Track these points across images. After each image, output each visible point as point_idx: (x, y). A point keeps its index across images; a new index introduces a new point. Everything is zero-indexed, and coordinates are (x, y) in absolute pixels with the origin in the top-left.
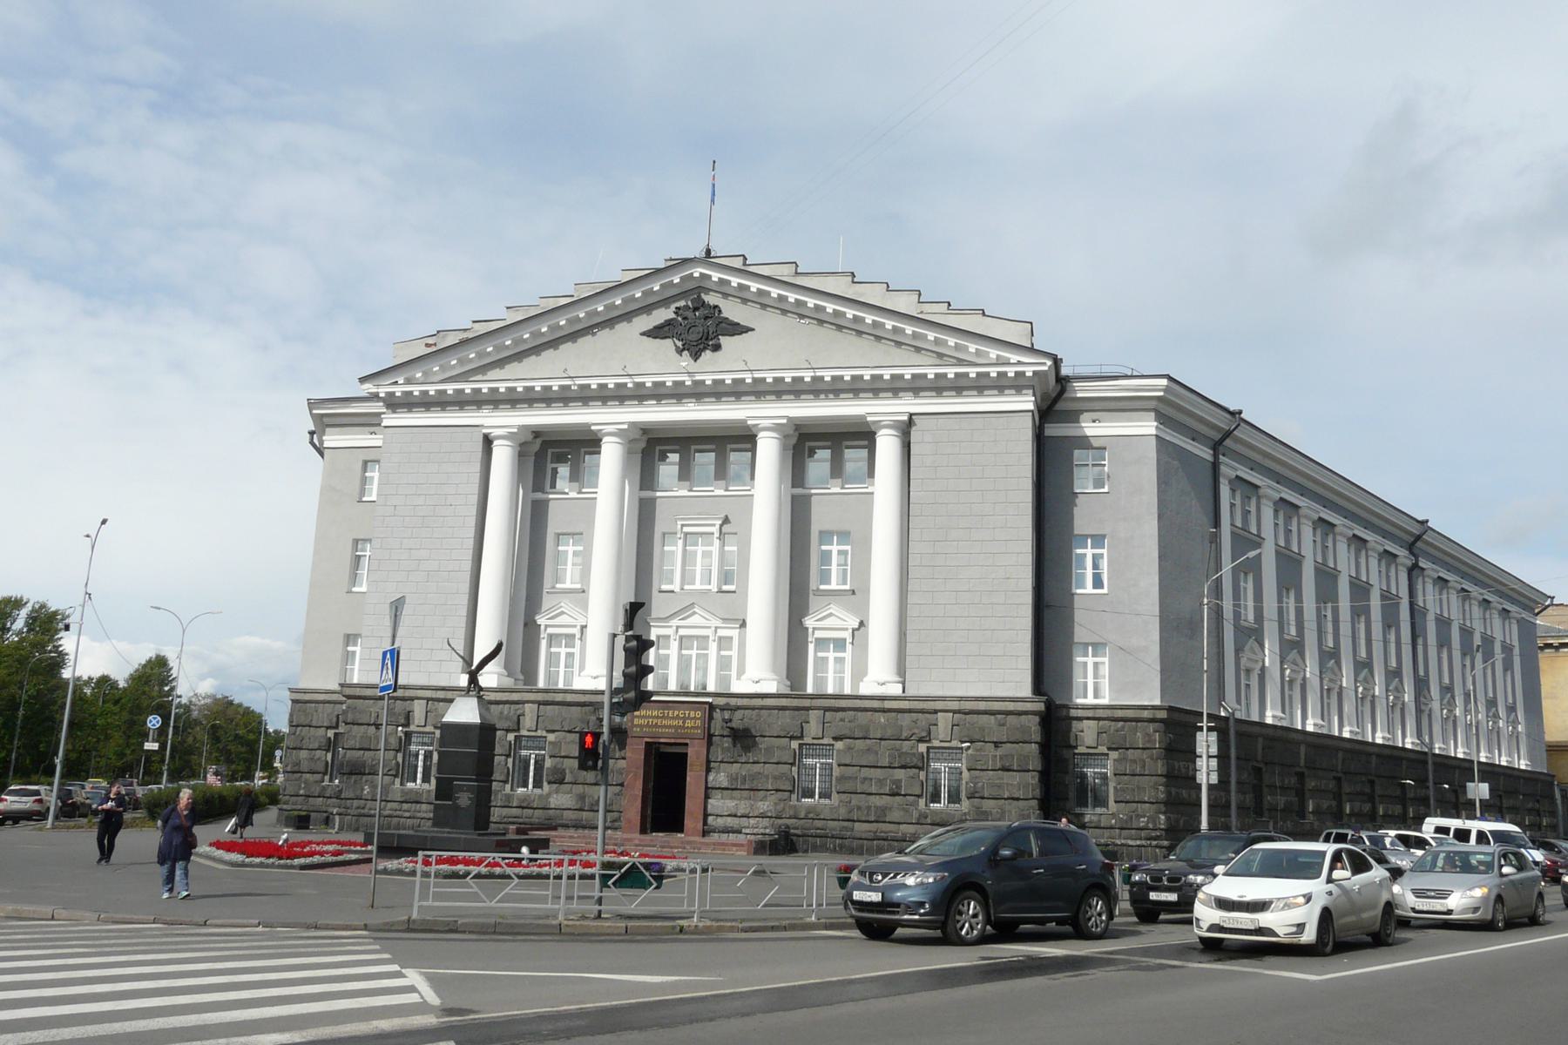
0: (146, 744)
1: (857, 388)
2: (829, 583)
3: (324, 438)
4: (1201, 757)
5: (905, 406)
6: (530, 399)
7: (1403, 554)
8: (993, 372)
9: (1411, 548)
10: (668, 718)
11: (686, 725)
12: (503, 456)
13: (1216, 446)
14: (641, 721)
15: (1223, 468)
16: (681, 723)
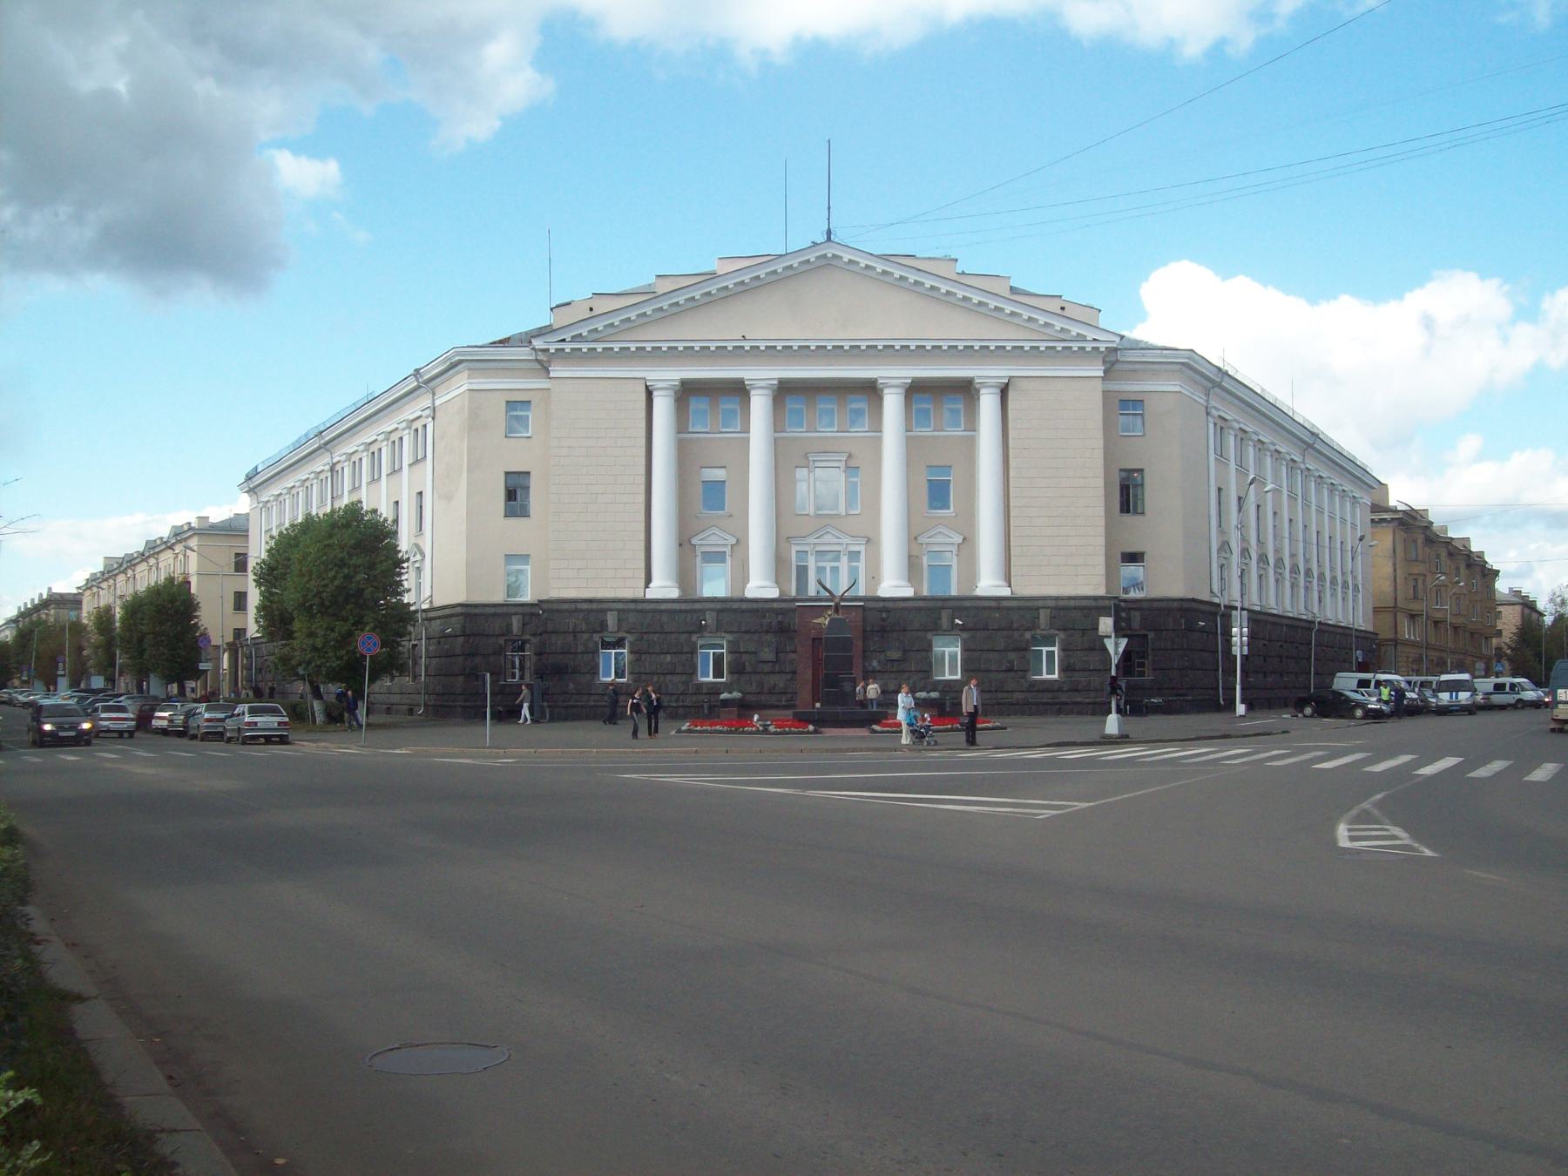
0: (201, 664)
1: (968, 353)
6: (688, 354)
7: (1285, 451)
12: (663, 407)
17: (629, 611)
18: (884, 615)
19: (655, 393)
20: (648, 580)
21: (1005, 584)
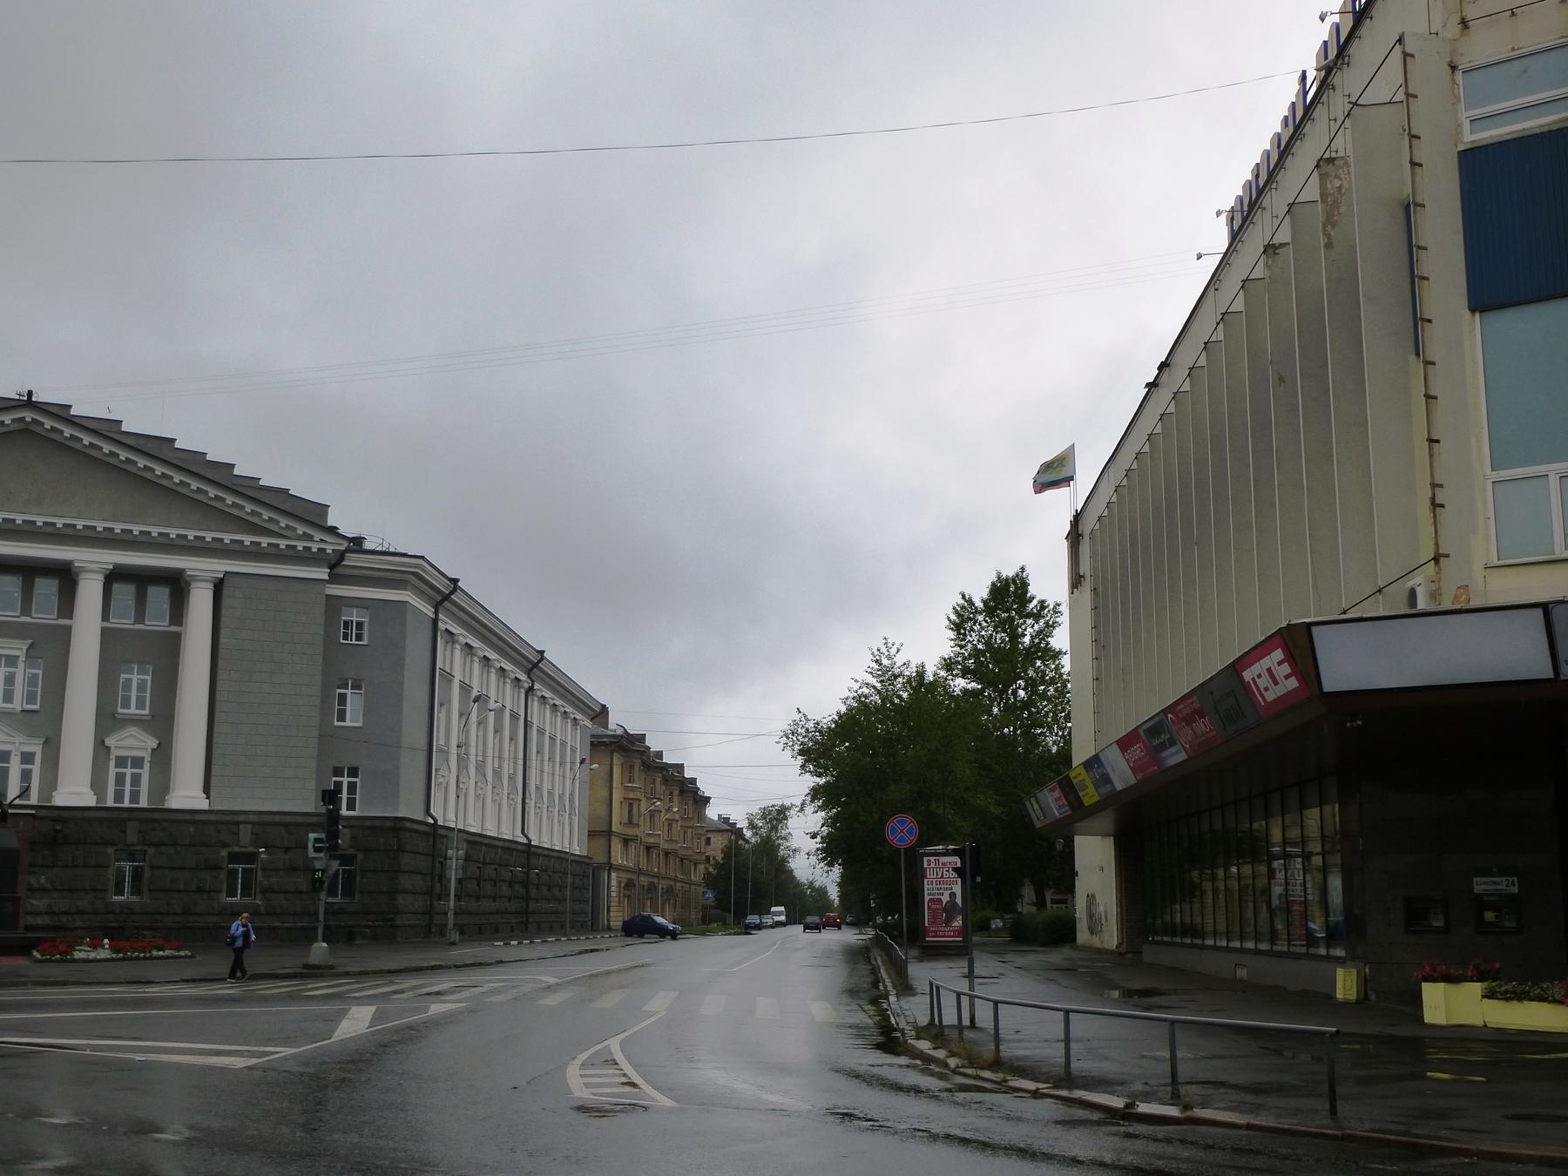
2: (129, 708)
4: (451, 859)
5: (219, 566)
8: (300, 545)
9: (529, 673)
13: (437, 607)
15: (440, 624)
21: (205, 796)
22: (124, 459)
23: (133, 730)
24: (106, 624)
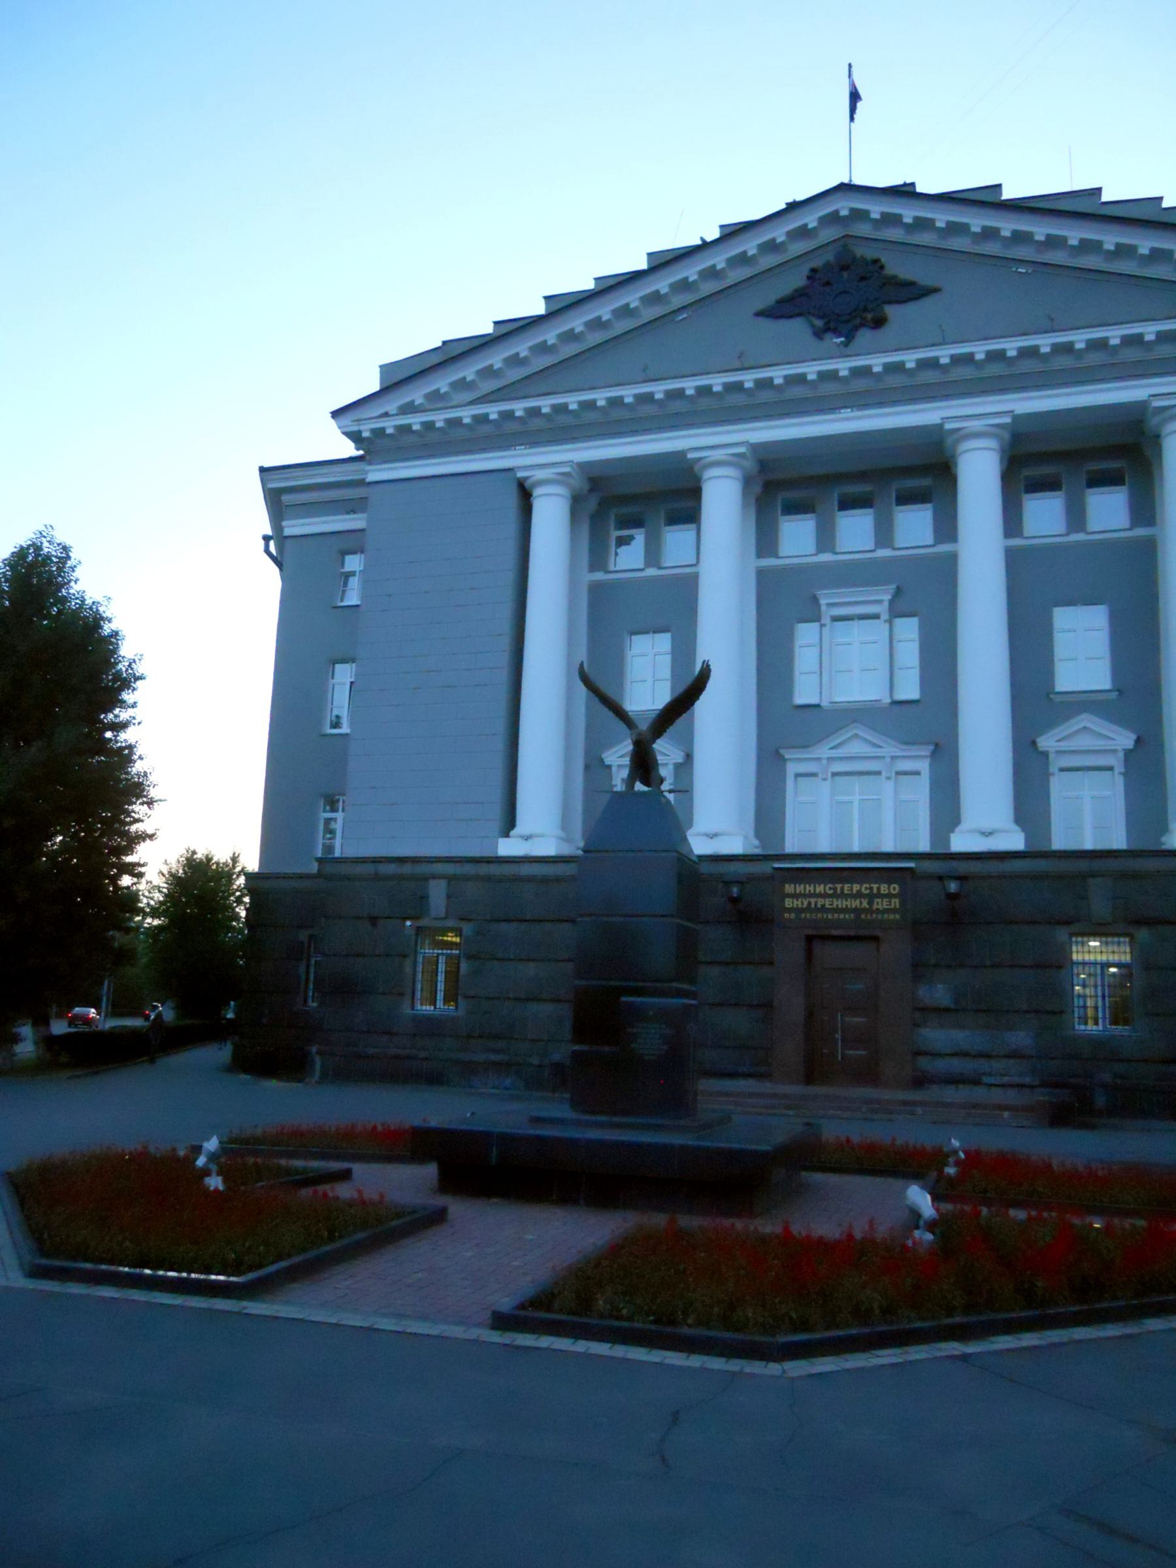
3: (284, 523)
10: (842, 895)
11: (875, 907)
14: (797, 903)
16: (865, 904)
17: (467, 878)
18: (953, 887)
19: (537, 492)
20: (509, 822)
22: (1042, 238)
23: (1085, 720)
24: (1016, 542)
